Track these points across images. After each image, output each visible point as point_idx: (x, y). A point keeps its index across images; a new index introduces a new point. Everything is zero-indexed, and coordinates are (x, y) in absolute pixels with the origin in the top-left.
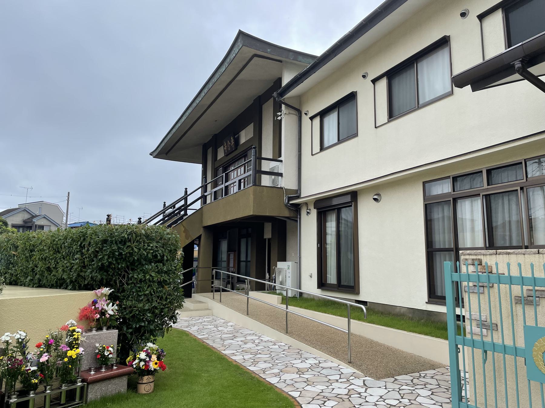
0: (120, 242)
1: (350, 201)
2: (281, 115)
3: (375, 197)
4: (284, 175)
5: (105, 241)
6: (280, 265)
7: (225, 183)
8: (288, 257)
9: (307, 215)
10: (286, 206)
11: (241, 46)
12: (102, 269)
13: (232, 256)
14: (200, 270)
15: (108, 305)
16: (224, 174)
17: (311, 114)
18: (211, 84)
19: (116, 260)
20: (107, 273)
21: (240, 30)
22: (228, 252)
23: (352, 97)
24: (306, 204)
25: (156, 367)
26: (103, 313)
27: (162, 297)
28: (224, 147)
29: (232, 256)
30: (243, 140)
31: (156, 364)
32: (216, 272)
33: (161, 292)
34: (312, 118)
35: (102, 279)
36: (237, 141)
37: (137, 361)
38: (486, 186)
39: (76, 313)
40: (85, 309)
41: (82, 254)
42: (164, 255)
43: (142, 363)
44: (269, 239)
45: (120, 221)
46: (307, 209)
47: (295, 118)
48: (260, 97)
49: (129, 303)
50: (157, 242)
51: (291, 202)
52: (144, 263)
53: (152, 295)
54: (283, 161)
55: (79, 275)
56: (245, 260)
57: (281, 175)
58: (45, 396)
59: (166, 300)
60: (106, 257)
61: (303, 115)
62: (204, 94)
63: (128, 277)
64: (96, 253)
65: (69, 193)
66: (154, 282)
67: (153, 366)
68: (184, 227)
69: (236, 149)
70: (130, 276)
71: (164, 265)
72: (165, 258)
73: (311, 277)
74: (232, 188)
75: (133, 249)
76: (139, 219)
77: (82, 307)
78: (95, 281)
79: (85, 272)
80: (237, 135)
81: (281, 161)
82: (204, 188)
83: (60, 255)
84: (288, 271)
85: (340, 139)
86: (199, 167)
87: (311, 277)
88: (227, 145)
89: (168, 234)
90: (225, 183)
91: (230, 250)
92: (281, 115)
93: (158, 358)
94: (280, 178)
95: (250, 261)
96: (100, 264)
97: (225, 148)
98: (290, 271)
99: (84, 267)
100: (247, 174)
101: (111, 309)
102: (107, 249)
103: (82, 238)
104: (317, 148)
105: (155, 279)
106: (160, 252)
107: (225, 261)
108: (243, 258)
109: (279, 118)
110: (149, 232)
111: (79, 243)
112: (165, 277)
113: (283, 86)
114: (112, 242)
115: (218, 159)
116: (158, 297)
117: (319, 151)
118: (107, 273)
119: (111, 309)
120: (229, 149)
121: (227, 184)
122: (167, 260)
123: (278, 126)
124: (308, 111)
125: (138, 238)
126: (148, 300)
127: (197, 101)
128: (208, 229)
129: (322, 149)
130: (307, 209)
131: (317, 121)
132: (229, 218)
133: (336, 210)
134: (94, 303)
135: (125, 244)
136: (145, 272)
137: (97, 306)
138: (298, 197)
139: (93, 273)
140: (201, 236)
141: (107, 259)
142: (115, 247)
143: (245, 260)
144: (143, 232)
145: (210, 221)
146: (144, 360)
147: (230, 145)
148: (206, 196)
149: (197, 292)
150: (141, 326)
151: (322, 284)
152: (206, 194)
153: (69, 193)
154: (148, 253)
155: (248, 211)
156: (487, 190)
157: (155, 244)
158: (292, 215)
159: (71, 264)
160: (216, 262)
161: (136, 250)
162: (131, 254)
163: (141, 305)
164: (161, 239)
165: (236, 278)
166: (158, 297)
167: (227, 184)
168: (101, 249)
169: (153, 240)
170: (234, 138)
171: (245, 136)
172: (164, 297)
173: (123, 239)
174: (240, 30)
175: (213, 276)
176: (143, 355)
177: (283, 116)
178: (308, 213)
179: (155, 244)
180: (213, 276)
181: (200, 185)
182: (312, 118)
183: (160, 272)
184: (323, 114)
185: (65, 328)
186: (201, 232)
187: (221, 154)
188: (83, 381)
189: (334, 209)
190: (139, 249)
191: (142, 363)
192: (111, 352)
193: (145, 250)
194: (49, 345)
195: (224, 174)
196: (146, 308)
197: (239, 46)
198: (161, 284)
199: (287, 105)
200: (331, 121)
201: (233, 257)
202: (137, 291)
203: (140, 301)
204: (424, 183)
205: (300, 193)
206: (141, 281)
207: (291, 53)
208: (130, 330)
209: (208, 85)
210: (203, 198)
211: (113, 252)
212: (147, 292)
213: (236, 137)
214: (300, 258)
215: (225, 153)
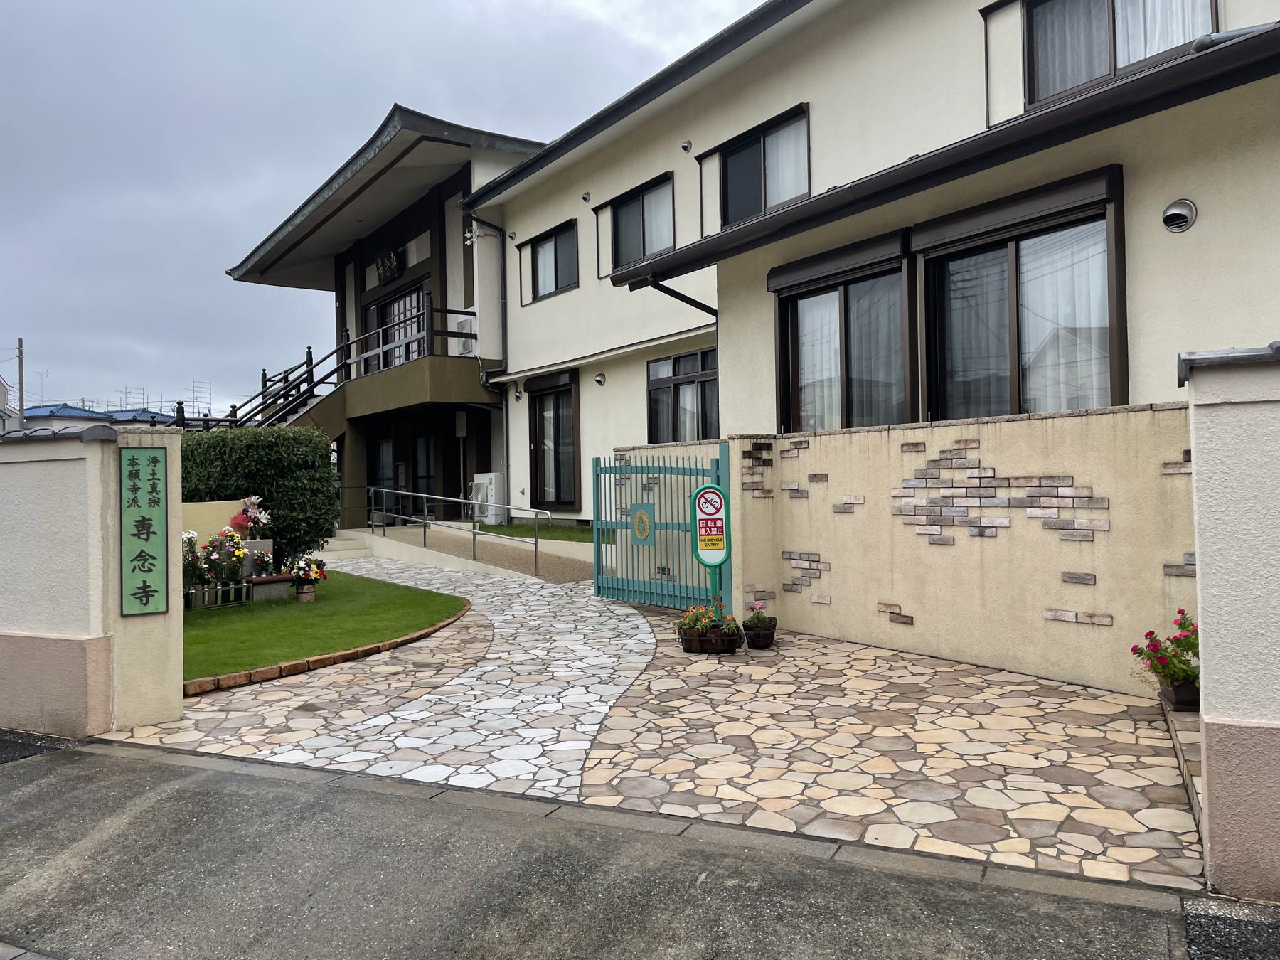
0: (267, 447)
1: (1104, 196)
2: (472, 237)
3: (598, 378)
4: (478, 337)
5: (250, 447)
6: (480, 478)
7: (383, 345)
8: (493, 468)
9: (517, 400)
10: (484, 386)
11: (399, 128)
12: (248, 476)
13: (402, 470)
14: (346, 491)
15: (260, 513)
16: (381, 330)
17: (519, 241)
18: (349, 172)
19: (265, 466)
20: (254, 480)
21: (395, 104)
22: (394, 462)
23: (569, 227)
24: (515, 382)
25: (316, 575)
26: (256, 521)
27: (316, 507)
28: (378, 268)
29: (402, 470)
30: (413, 260)
31: (316, 573)
32: (375, 491)
33: (315, 501)
34: (520, 247)
35: (249, 487)
36: (402, 259)
37: (295, 570)
38: (700, 372)
39: (229, 521)
40: (235, 518)
41: (223, 461)
42: (314, 461)
43: (301, 573)
44: (464, 438)
45: (136, 401)
46: (517, 392)
47: (493, 242)
48: (439, 186)
49: (281, 512)
50: (307, 446)
51: (491, 381)
52: (294, 469)
53: (305, 503)
54: (477, 315)
55: (219, 485)
56: (425, 474)
57: (474, 336)
58: (216, 592)
59: (321, 509)
60: (254, 464)
61: (508, 240)
62: (337, 186)
63: (277, 485)
64: (241, 459)
65: (21, 341)
66: (306, 490)
67: (313, 575)
68: (313, 420)
69: (401, 275)
70: (280, 483)
71: (316, 472)
72: (317, 464)
73: (523, 493)
74: (397, 333)
75: (282, 455)
76: (232, 407)
77: (232, 516)
78: (240, 489)
79: (228, 481)
80: (402, 248)
81: (474, 314)
82: (343, 350)
83: (191, 463)
84: (490, 487)
85: (559, 287)
86: (330, 297)
87: (523, 493)
88: (383, 265)
89: (317, 437)
90: (383, 345)
91: (396, 458)
92: (472, 237)
93: (318, 568)
94: (474, 340)
95: (433, 477)
96: (247, 471)
97: (381, 272)
98: (493, 486)
99: (227, 475)
100: (420, 335)
101: (264, 518)
102: (254, 455)
103: (221, 444)
104: (528, 297)
105: (308, 487)
106: (311, 457)
107: (390, 479)
108: (422, 471)
109: (468, 242)
110: (297, 436)
111: (218, 449)
112: (317, 485)
113: (473, 192)
114: (258, 446)
115: (367, 289)
116: (312, 506)
117: (531, 301)
118: (254, 480)
119: (264, 518)
120: (388, 274)
121: (387, 348)
122: (319, 466)
123: (468, 251)
124: (514, 233)
125: (287, 442)
126: (301, 509)
127: (326, 195)
128: (355, 423)
129: (536, 298)
130: (517, 392)
131: (527, 252)
132: (393, 406)
133: (553, 395)
134: (245, 511)
135: (272, 450)
136: (296, 480)
137: (249, 514)
138: (504, 373)
139: (239, 482)
140: (344, 434)
141: (255, 466)
142: (263, 453)
143: (425, 474)
144: (291, 435)
145: (359, 409)
146: (303, 569)
147: (389, 267)
148: (349, 365)
149: (343, 527)
150: (296, 536)
151: (537, 500)
152: (348, 361)
153: (21, 341)
154: (298, 458)
155: (423, 395)
156: (701, 376)
157: (303, 449)
158: (494, 400)
159: (209, 472)
160: (373, 477)
161: (286, 456)
162: (281, 460)
163: (295, 514)
164: (310, 442)
165: (411, 499)
166: (312, 506)
167: (387, 348)
168: (247, 456)
169: (301, 443)
170: (397, 255)
171: (417, 252)
172: (319, 507)
173: (271, 443)
174: (395, 104)
175: (369, 499)
176: (302, 564)
177: (474, 239)
178: (518, 398)
179: (305, 449)
180: (369, 499)
181: (335, 348)
182: (520, 247)
183: (312, 479)
184: (536, 243)
185: (222, 534)
186: (345, 427)
187: (372, 281)
188: (247, 582)
189: (550, 394)
190: (289, 455)
191: (301, 573)
192: (269, 558)
193: (295, 455)
194: (215, 546)
195: (381, 330)
196: (300, 517)
197: (395, 127)
198: (315, 492)
199: (480, 221)
200: (547, 254)
201: (403, 471)
202: (289, 499)
203: (293, 509)
204: (648, 363)
205: (507, 365)
206: (293, 489)
207: (483, 137)
208: (284, 541)
209: (344, 172)
210: (343, 369)
211: (261, 458)
212: (300, 501)
213: (399, 250)
214: (508, 466)
215: (380, 280)
